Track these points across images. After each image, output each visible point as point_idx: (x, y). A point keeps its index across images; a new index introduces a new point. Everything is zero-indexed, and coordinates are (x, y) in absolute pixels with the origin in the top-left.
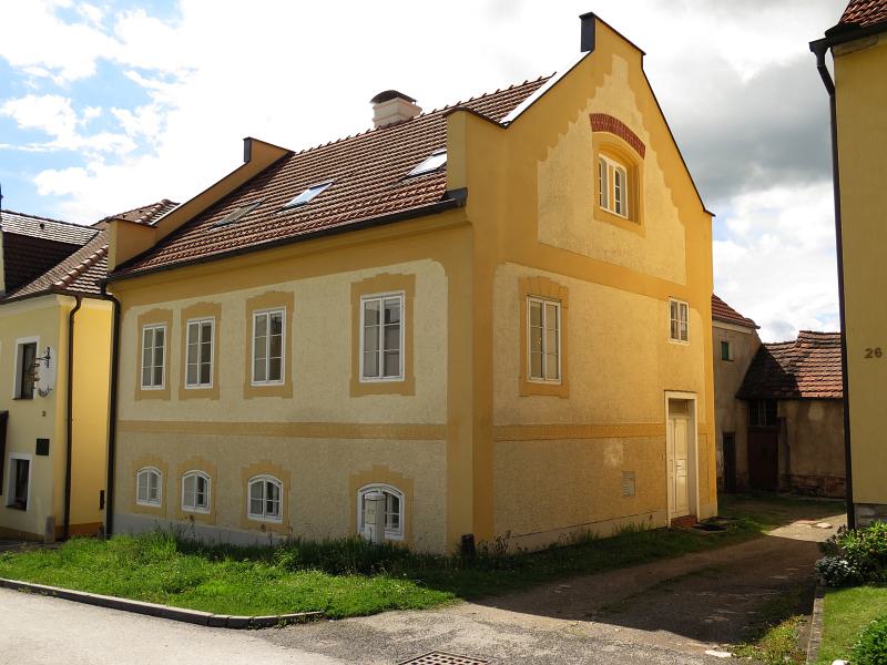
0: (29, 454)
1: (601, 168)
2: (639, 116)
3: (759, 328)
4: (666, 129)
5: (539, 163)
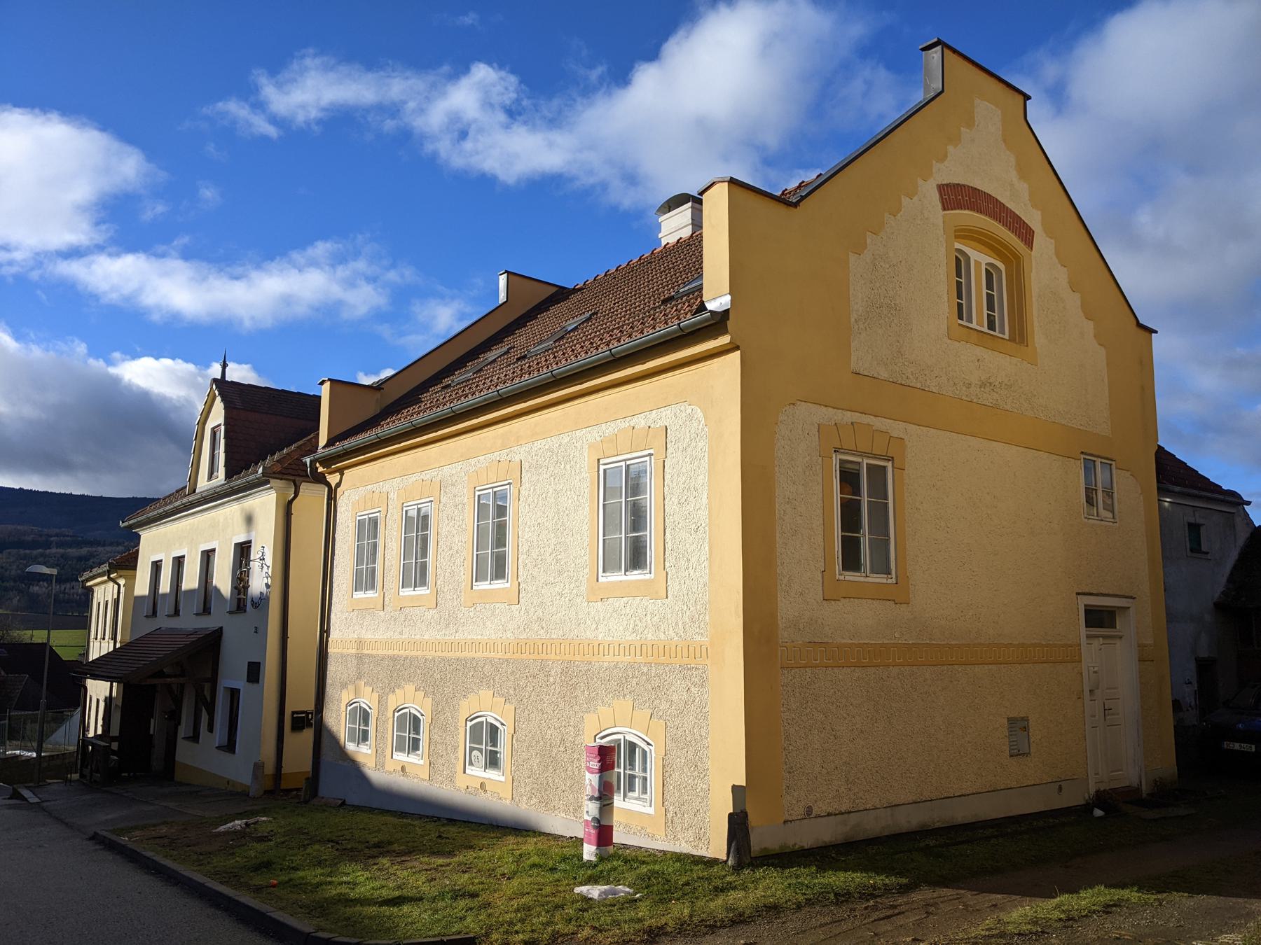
0: (240, 683)
1: (960, 265)
2: (1023, 187)
3: (1249, 503)
4: (1067, 202)
5: (853, 258)
